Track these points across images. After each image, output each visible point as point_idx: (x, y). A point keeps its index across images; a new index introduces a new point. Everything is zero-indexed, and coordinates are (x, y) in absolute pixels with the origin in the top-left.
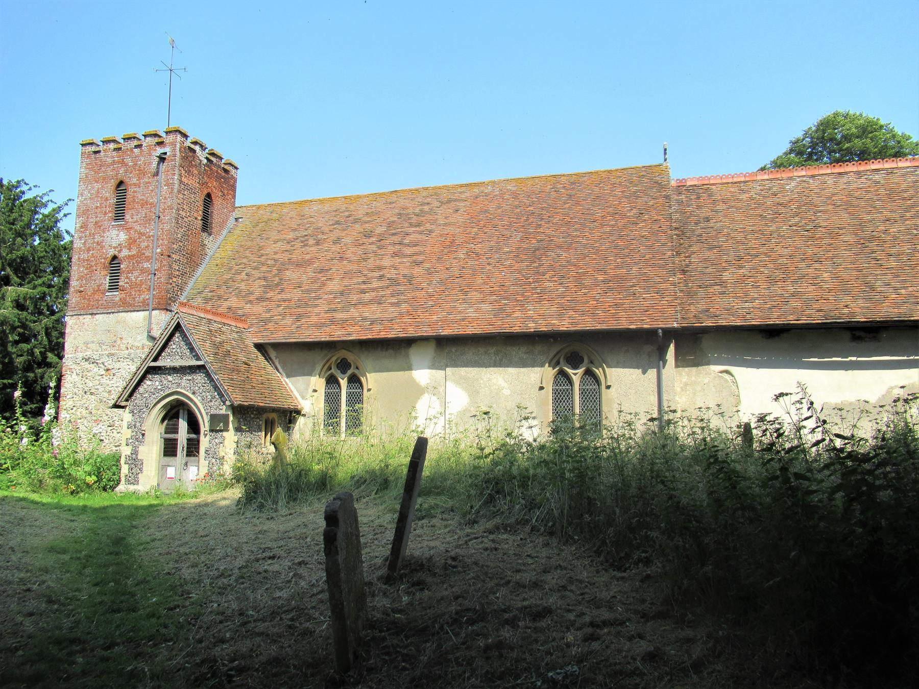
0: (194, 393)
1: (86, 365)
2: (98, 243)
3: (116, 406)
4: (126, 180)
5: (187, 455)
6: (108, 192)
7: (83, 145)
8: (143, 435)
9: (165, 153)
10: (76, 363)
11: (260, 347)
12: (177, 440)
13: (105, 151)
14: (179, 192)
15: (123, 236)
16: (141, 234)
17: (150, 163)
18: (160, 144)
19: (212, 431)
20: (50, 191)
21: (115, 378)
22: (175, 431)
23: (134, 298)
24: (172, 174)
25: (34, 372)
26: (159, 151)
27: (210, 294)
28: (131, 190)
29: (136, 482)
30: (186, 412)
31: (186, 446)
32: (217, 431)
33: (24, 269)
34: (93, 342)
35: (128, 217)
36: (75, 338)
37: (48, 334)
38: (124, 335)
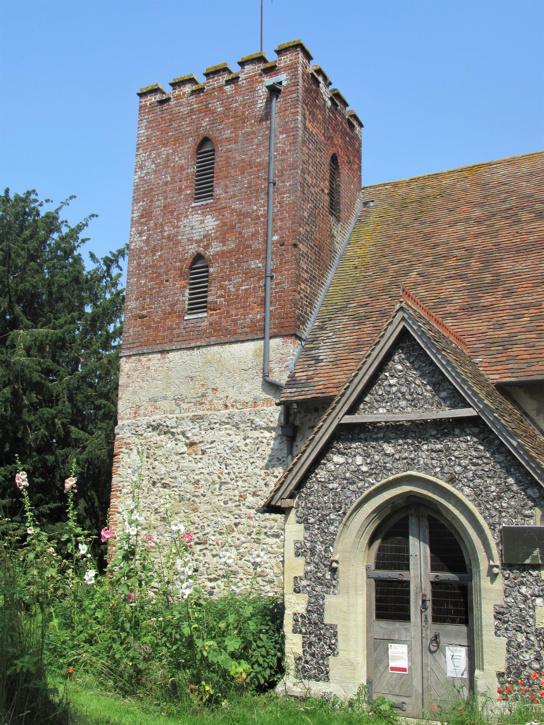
0: (452, 480)
1: (154, 437)
2: (169, 238)
3: (270, 508)
4: (212, 134)
5: (435, 620)
6: (184, 158)
7: (141, 95)
8: (334, 571)
9: (280, 83)
10: (137, 434)
11: (504, 389)
12: (407, 583)
13: (177, 98)
14: (304, 142)
15: (211, 223)
16: (242, 215)
17: (254, 103)
18: (271, 70)
19: (507, 566)
20: (71, 198)
21: (205, 457)
22: (403, 563)
23: (235, 322)
24: (290, 114)
25: (53, 453)
26: (269, 81)
27: (361, 310)
28: (221, 151)
29: (323, 674)
30: (425, 523)
31: (429, 596)
32: (524, 568)
33: (34, 308)
34: (165, 398)
35: (218, 191)
36: (134, 393)
37: (71, 399)
38: (220, 383)
